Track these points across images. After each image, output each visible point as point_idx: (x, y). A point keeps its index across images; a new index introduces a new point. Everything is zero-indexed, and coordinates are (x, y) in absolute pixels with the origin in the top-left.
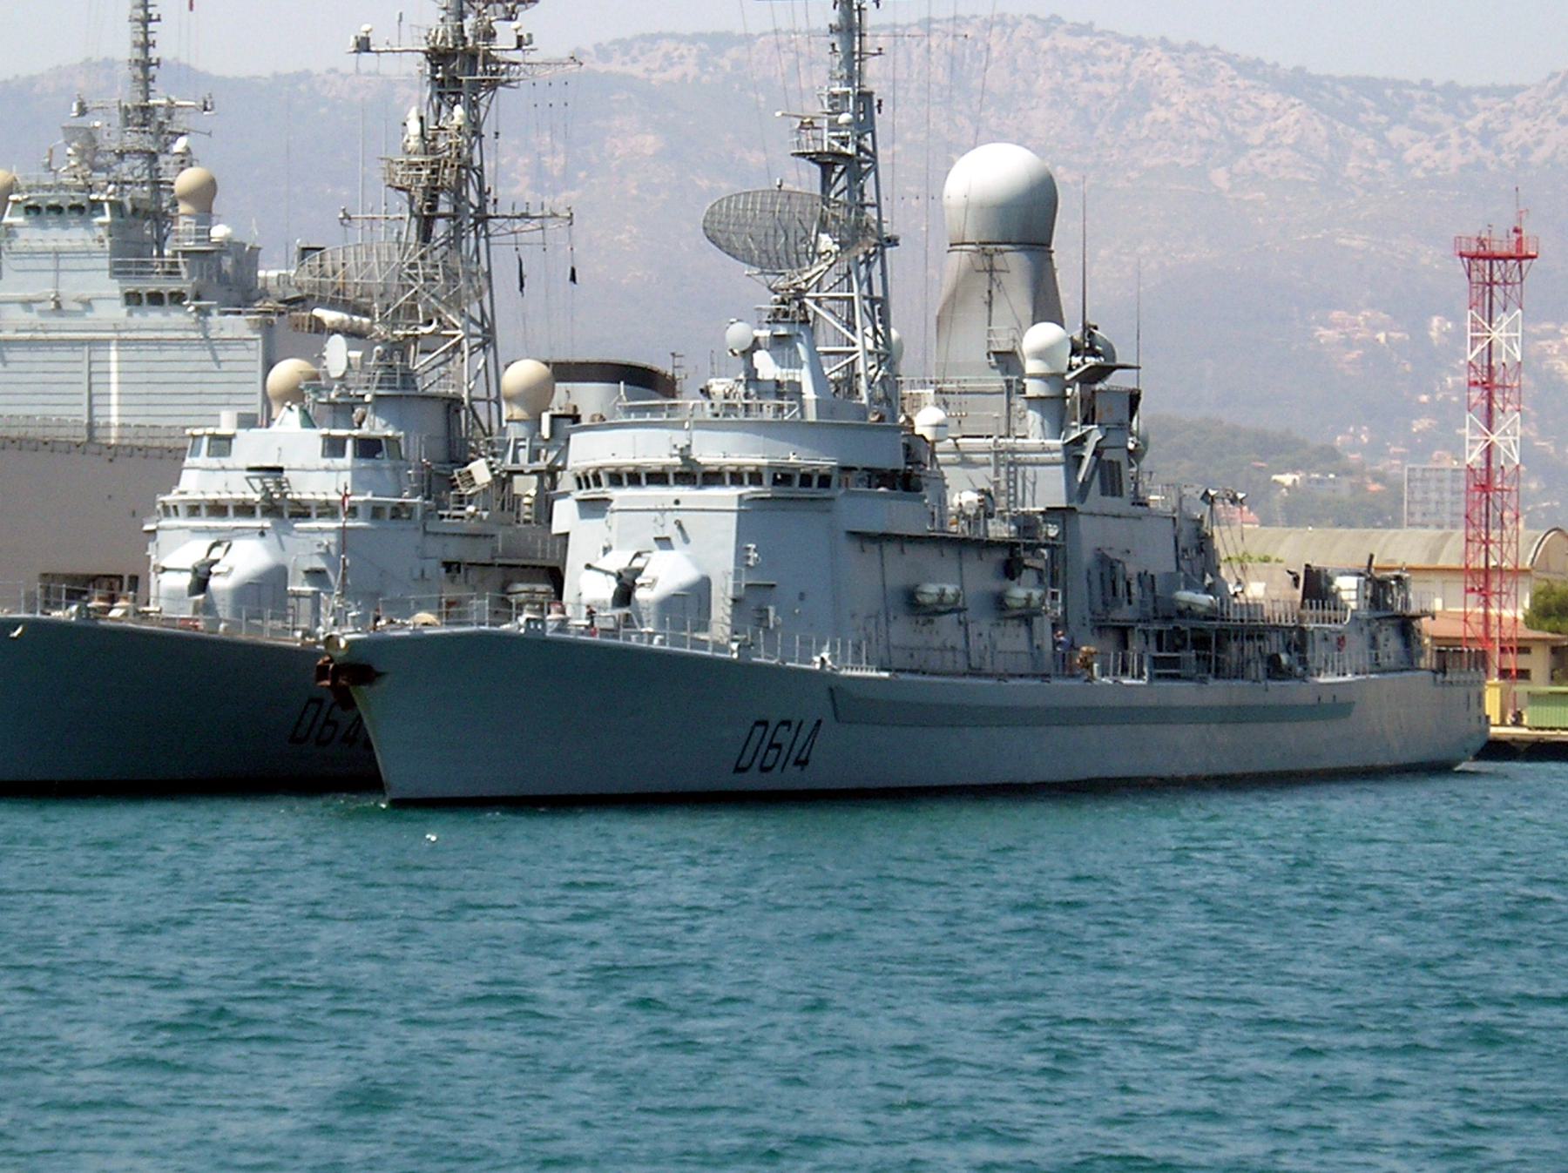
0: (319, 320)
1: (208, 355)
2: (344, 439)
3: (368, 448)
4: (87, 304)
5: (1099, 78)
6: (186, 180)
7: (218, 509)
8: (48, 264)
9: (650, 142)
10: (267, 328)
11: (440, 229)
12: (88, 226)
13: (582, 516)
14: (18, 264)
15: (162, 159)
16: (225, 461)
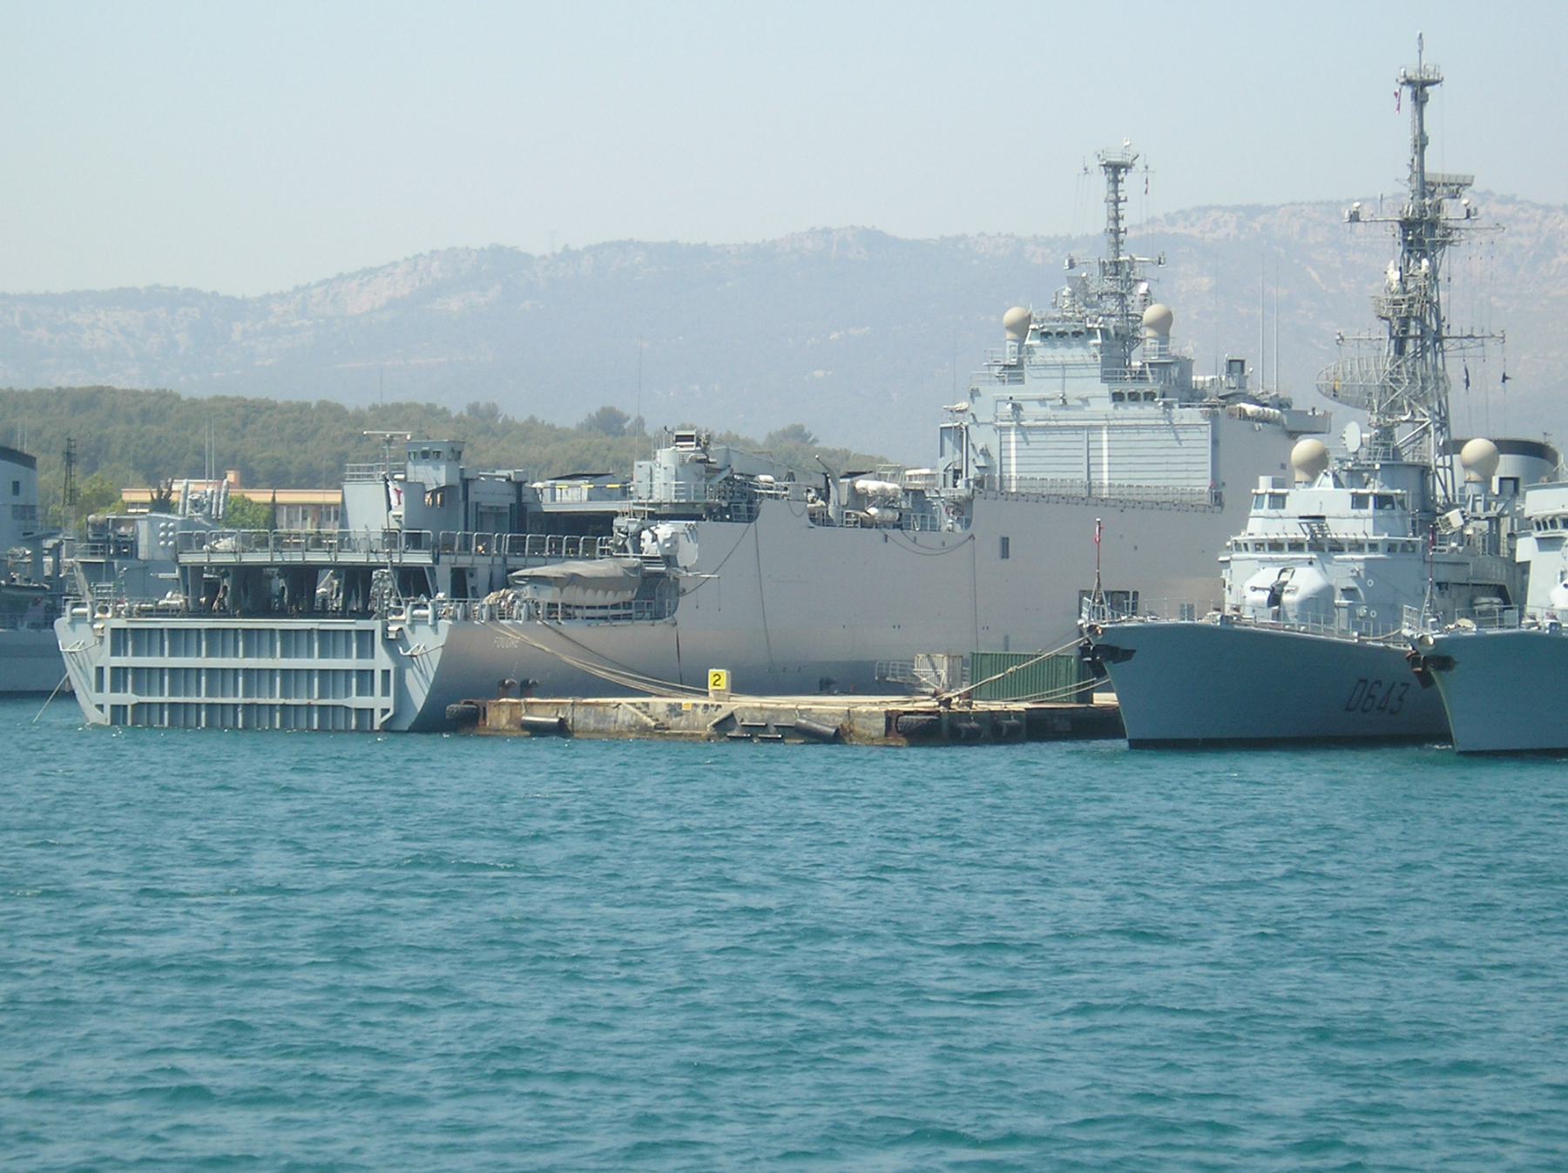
0: (1242, 411)
1: (1172, 436)
2: (1367, 495)
3: (1382, 501)
4: (1085, 401)
5: (1520, 234)
6: (1151, 313)
7: (1276, 546)
8: (1058, 373)
9: (1206, 282)
10: (1214, 417)
11: (1410, 347)
12: (1085, 346)
13: (1541, 549)
14: (1036, 373)
15: (1130, 298)
16: (1281, 512)
